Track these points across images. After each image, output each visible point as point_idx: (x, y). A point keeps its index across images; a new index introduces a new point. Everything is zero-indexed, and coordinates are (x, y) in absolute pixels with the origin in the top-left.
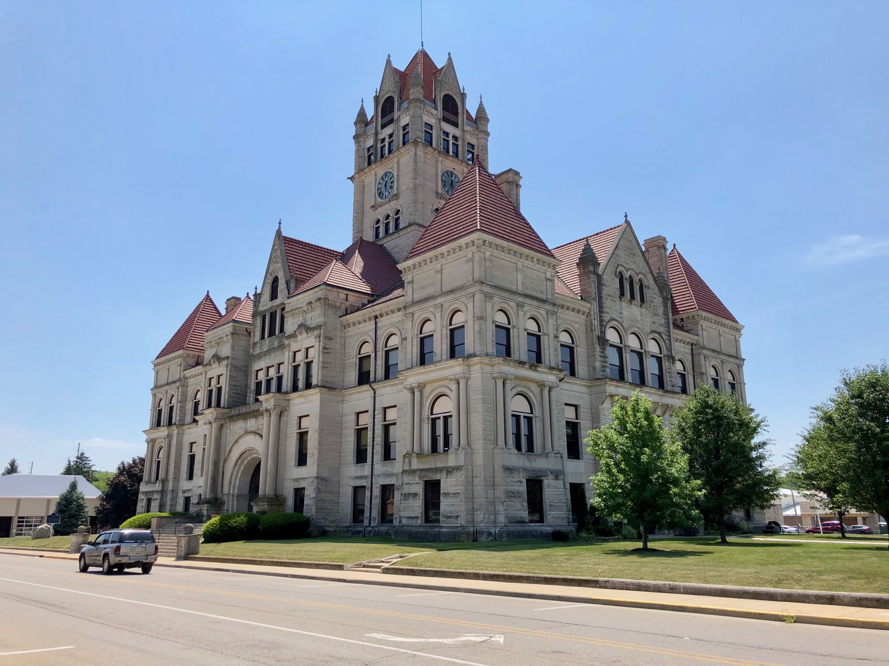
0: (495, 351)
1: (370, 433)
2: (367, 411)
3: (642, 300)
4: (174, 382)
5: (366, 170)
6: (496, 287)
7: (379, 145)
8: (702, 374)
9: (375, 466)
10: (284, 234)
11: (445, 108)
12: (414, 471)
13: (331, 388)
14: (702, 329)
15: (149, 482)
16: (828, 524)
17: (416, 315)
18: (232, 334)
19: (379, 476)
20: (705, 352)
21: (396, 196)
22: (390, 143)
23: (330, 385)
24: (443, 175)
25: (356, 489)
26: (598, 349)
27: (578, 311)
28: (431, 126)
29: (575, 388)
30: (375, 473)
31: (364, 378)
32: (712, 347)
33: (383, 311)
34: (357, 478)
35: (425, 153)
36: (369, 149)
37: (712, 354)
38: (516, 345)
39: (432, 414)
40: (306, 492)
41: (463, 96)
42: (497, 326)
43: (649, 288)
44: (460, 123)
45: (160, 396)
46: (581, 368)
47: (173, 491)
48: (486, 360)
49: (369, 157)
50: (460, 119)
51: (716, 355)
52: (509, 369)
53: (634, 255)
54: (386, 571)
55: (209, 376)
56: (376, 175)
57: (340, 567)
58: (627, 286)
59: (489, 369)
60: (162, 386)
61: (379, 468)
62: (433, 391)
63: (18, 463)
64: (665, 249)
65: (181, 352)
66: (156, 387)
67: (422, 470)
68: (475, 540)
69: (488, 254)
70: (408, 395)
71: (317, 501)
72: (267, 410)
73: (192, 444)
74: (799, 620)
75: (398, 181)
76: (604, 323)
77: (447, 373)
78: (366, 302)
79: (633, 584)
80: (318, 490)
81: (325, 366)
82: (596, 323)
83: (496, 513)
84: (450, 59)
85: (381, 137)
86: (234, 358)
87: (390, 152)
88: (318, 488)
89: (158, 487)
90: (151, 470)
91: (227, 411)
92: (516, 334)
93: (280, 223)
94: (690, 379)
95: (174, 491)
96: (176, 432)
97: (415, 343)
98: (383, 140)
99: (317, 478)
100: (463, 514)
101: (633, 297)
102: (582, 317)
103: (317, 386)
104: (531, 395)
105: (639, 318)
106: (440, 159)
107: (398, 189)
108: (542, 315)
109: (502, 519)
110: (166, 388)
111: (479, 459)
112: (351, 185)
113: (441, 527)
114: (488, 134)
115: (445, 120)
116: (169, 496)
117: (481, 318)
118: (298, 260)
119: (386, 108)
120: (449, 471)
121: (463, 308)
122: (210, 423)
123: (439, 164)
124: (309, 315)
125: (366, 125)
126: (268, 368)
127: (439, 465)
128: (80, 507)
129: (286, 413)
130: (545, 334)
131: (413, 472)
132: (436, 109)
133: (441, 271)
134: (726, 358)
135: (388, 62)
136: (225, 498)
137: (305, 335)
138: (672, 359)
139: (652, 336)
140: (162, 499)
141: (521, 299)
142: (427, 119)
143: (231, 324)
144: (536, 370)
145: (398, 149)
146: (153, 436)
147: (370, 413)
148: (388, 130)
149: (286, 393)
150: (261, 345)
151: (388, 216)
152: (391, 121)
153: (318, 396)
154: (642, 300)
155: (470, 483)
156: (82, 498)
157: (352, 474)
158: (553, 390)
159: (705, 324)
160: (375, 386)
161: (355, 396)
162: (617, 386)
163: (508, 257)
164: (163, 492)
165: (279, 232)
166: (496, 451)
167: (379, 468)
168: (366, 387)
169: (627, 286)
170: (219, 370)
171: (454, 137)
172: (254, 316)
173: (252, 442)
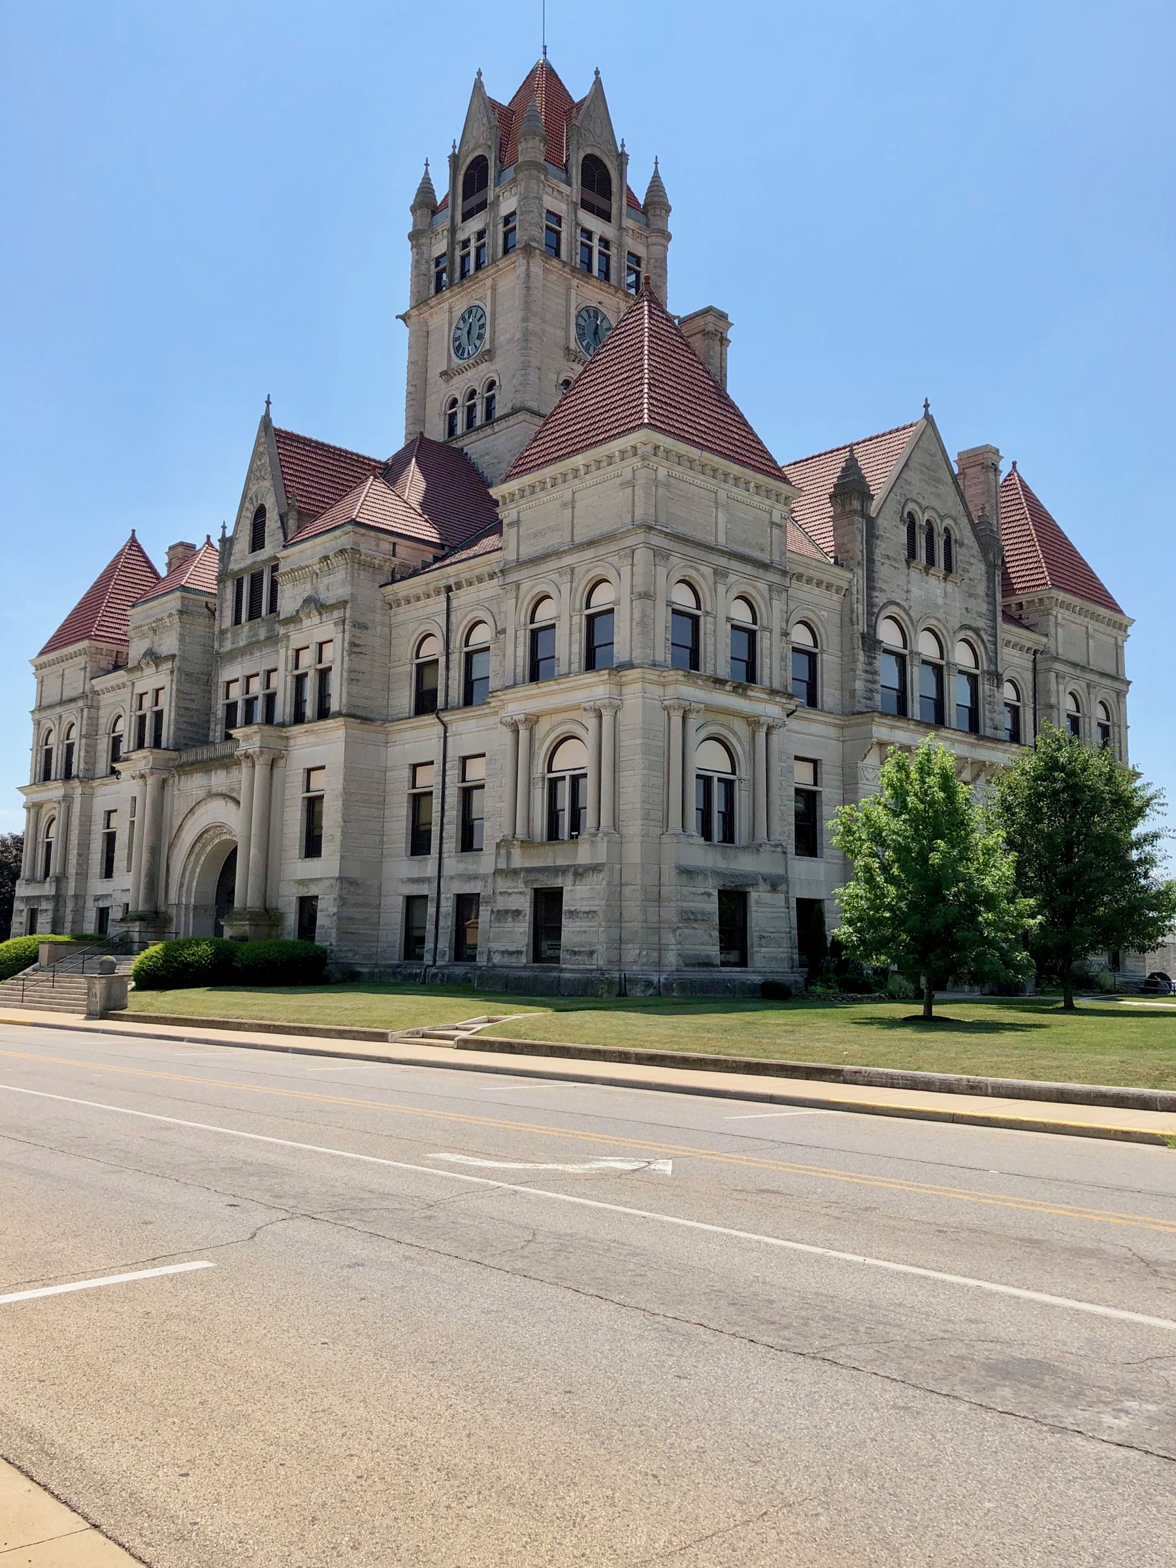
4: (73, 700)
5: (433, 302)
7: (458, 253)
8: (1051, 707)
9: (446, 861)
10: (276, 424)
11: (586, 182)
12: (516, 872)
13: (365, 720)
14: (1057, 624)
15: (31, 880)
19: (452, 878)
20: (1058, 666)
22: (479, 250)
23: (363, 714)
24: (579, 315)
26: (861, 657)
30: (446, 872)
31: (425, 703)
32: (1072, 658)
33: (463, 577)
36: (438, 261)
40: (321, 905)
41: (622, 159)
43: (962, 545)
44: (614, 211)
46: (828, 693)
47: (76, 896)
48: (652, 675)
49: (440, 276)
53: (939, 480)
54: (464, 1045)
55: (139, 690)
57: (382, 1037)
59: (657, 691)
60: (51, 707)
64: (996, 470)
65: (85, 644)
66: (40, 708)
67: (529, 870)
68: (622, 994)
70: (508, 735)
71: (340, 919)
76: (876, 610)
78: (430, 559)
79: (903, 1077)
80: (342, 901)
81: (353, 677)
82: (860, 608)
83: (661, 949)
84: (598, 83)
85: (461, 236)
86: (184, 659)
87: (479, 266)
89: (48, 889)
91: (174, 754)
93: (268, 403)
94: (1027, 716)
96: (79, 791)
98: (466, 244)
99: (340, 879)
100: (601, 949)
101: (931, 561)
102: (836, 597)
103: (339, 714)
104: (733, 740)
105: (940, 601)
106: (575, 282)
107: (492, 340)
108: (762, 596)
110: (58, 710)
111: (634, 853)
112: (403, 333)
113: (561, 970)
114: (668, 237)
115: (587, 205)
118: (303, 475)
119: (473, 178)
120: (579, 872)
122: (143, 776)
123: (573, 292)
126: (248, 678)
127: (561, 862)
129: (281, 763)
130: (764, 629)
133: (573, 504)
135: (478, 86)
136: (173, 911)
137: (316, 619)
138: (996, 678)
140: (56, 911)
141: (723, 561)
143: (178, 594)
147: (438, 766)
149: (283, 725)
151: (473, 394)
152: (482, 206)
153: (341, 733)
154: (949, 568)
157: (403, 874)
158: (775, 732)
159: (1061, 614)
160: (446, 717)
161: (408, 735)
162: (892, 727)
163: (699, 480)
164: (58, 898)
165: (266, 421)
166: (666, 839)
168: (429, 719)
170: (153, 679)
171: (601, 239)
172: (221, 579)
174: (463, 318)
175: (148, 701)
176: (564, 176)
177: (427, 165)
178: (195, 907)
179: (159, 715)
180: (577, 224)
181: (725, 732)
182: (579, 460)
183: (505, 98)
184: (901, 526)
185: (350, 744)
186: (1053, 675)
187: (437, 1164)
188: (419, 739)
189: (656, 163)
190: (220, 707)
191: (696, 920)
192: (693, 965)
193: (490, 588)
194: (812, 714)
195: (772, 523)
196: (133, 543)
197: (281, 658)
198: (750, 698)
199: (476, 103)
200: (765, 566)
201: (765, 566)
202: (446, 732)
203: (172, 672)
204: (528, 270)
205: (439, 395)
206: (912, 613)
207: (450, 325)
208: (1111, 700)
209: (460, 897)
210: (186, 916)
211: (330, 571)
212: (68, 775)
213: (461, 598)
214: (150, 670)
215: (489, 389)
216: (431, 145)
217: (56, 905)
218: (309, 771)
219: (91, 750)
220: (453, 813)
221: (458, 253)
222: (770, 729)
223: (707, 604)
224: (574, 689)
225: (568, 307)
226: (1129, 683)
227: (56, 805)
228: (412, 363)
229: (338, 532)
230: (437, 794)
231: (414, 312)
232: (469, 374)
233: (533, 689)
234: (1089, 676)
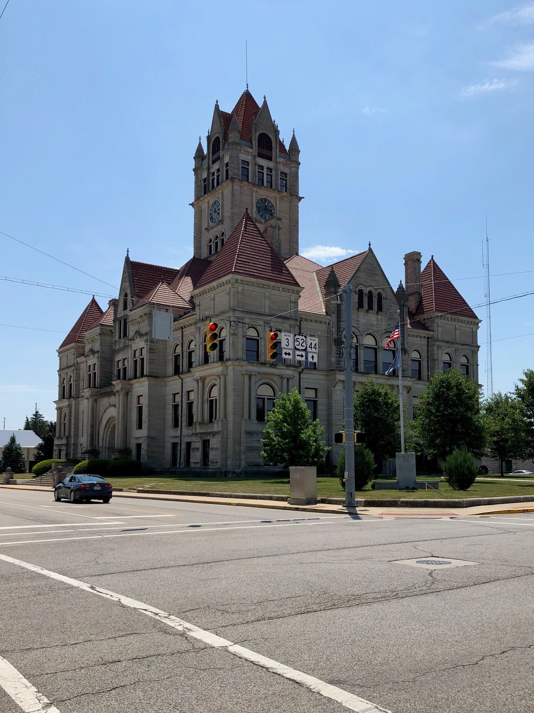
0: (245, 356)
1: (180, 407)
2: (178, 393)
3: (380, 309)
4: (70, 367)
5: (202, 199)
7: (211, 178)
8: (434, 360)
9: (183, 430)
10: (131, 259)
11: (260, 145)
12: (197, 434)
13: (156, 377)
15: (58, 438)
17: (202, 329)
18: (100, 334)
19: (185, 436)
21: (221, 222)
22: (218, 177)
23: (155, 375)
26: (334, 348)
27: (321, 322)
28: (248, 163)
29: (315, 377)
30: (183, 434)
31: (177, 371)
33: (186, 323)
34: (174, 437)
35: (240, 186)
36: (205, 180)
37: (445, 344)
38: (263, 351)
39: (210, 397)
40: (142, 447)
41: (276, 132)
42: (247, 338)
43: (386, 299)
44: (274, 156)
47: (74, 444)
48: (236, 363)
49: (205, 187)
50: (274, 153)
51: (450, 345)
52: (254, 368)
53: (375, 274)
54: (139, 491)
56: (208, 203)
57: (121, 490)
59: (240, 368)
60: (64, 369)
62: (209, 382)
64: (419, 262)
67: (201, 433)
68: (226, 476)
69: (240, 288)
70: (195, 383)
71: (148, 452)
72: (118, 392)
73: (139, 397)
74: (238, 505)
75: (222, 207)
78: (183, 314)
79: (219, 494)
80: (149, 445)
81: (151, 362)
82: (334, 330)
83: (240, 460)
85: (212, 171)
87: (218, 184)
88: (148, 444)
89: (64, 442)
90: (60, 430)
91: (99, 390)
92: (263, 343)
93: (128, 251)
94: (424, 364)
96: (74, 403)
97: (201, 348)
98: (213, 174)
99: (148, 437)
100: (219, 461)
101: (370, 307)
103: (147, 376)
105: (375, 323)
106: (255, 189)
107: (222, 215)
110: (66, 370)
111: (231, 427)
112: (192, 210)
113: (209, 469)
114: (299, 164)
115: (260, 155)
116: (72, 448)
117: (234, 334)
119: (216, 143)
120: (214, 434)
121: (193, 339)
122: (88, 398)
123: (254, 193)
124: (142, 325)
125: (203, 160)
126: (124, 359)
128: (19, 455)
129: (130, 393)
132: (252, 148)
133: (214, 299)
134: (460, 347)
135: (217, 107)
136: (100, 450)
137: (139, 339)
140: (67, 450)
142: (243, 157)
143: (99, 327)
144: (275, 368)
145: (222, 182)
146: (61, 405)
148: (216, 166)
149: (130, 379)
150: (120, 342)
151: (217, 237)
152: (218, 159)
153: (147, 383)
154: (380, 309)
156: (20, 449)
157: (171, 434)
158: (290, 380)
159: (440, 322)
161: (172, 382)
163: (257, 289)
164: (67, 445)
165: (127, 259)
166: (243, 422)
168: (176, 377)
170: (93, 360)
171: (267, 168)
173: (112, 412)
174: (213, 206)
175: (138, 353)
176: (249, 144)
177: (200, 139)
178: (108, 448)
179: (142, 360)
180: (256, 164)
181: (269, 381)
182: (214, 284)
184: (355, 295)
185: (151, 388)
186: (436, 347)
187: (42, 507)
188: (174, 385)
189: (294, 131)
190: (115, 371)
191: (253, 450)
192: (252, 466)
193: (192, 329)
195: (291, 302)
196: (94, 301)
197: (129, 354)
198: (277, 368)
199: (216, 115)
202: (182, 382)
203: (98, 358)
204: (233, 187)
205: (206, 237)
206: (359, 329)
207: (208, 208)
208: (469, 355)
210: (105, 451)
211: (143, 321)
212: (70, 396)
213: (186, 331)
215: (222, 236)
217: (67, 447)
219: (78, 386)
220: (185, 412)
221: (211, 178)
222: (288, 380)
223: (261, 335)
224: (213, 368)
225: (252, 200)
226: (479, 347)
228: (195, 224)
229: (144, 307)
230: (180, 405)
231: (196, 203)
232: (215, 229)
234: (455, 346)
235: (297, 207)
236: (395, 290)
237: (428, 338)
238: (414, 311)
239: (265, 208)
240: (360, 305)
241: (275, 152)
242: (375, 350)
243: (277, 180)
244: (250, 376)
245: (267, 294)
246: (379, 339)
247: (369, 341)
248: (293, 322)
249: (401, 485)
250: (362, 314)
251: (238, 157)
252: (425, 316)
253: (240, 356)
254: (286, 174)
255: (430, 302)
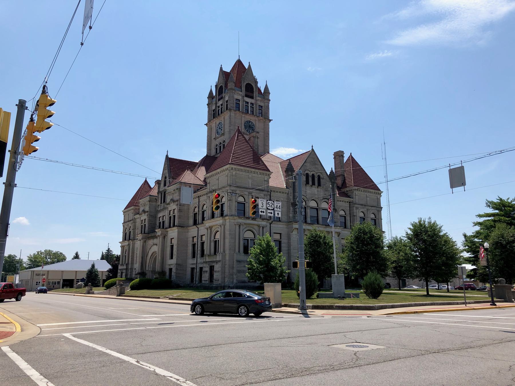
0: (236, 213)
3: (319, 185)
5: (212, 121)
6: (238, 187)
7: (217, 109)
10: (169, 157)
16: (466, 285)
18: (149, 201)
20: (356, 206)
22: (221, 108)
24: (245, 123)
25: (193, 269)
26: (291, 208)
27: (283, 193)
30: (198, 262)
31: (195, 223)
32: (361, 203)
36: (214, 111)
37: (361, 206)
41: (256, 82)
43: (323, 179)
44: (254, 96)
45: (126, 226)
48: (231, 218)
49: (214, 114)
50: (254, 95)
53: (316, 164)
54: (170, 299)
55: (169, 210)
57: (159, 298)
58: (310, 179)
59: (233, 221)
61: (199, 260)
63: (79, 253)
64: (343, 157)
65: (133, 207)
66: (124, 223)
67: (209, 262)
69: (234, 173)
77: (218, 223)
80: (177, 269)
81: (179, 217)
82: (291, 197)
84: (250, 65)
85: (218, 105)
87: (222, 112)
89: (125, 267)
94: (348, 218)
95: (132, 269)
98: (219, 107)
100: (220, 279)
101: (313, 184)
102: (285, 195)
103: (176, 226)
104: (254, 230)
105: (316, 193)
106: (243, 115)
109: (235, 281)
112: (206, 128)
115: (247, 96)
116: (129, 271)
117: (230, 200)
118: (175, 167)
119: (220, 89)
120: (217, 262)
124: (175, 195)
127: (214, 260)
128: (97, 275)
131: (206, 262)
132: (242, 91)
134: (370, 208)
136: (147, 272)
139: (324, 200)
140: (126, 272)
142: (236, 97)
145: (224, 111)
146: (123, 245)
147: (197, 237)
148: (220, 102)
152: (222, 98)
153: (177, 230)
154: (319, 185)
155: (223, 267)
156: (97, 271)
157: (191, 262)
159: (357, 193)
160: (198, 226)
161: (192, 230)
163: (244, 173)
165: (167, 156)
167: (199, 260)
168: (195, 227)
169: (310, 179)
170: (144, 217)
172: (158, 193)
173: (155, 249)
181: (251, 229)
182: (219, 170)
183: (228, 70)
186: (355, 208)
188: (193, 231)
194: (279, 223)
196: (146, 181)
197: (166, 213)
200: (263, 191)
201: (263, 191)
205: (214, 143)
208: (376, 213)
209: (293, 262)
211: (176, 193)
213: (202, 199)
214: (143, 215)
216: (212, 80)
218: (172, 239)
219: (134, 233)
220: (199, 248)
221: (217, 109)
227: (219, 227)
233: (213, 220)
235: (268, 125)
236: (328, 173)
237: (350, 202)
238: (340, 186)
239: (249, 126)
240: (307, 182)
241: (256, 94)
242: (317, 209)
243: (256, 110)
244: (240, 226)
245: (250, 176)
246: (319, 203)
247: (313, 204)
248: (266, 193)
249: (335, 295)
250: (308, 187)
251: (233, 97)
252: (347, 189)
253: (233, 213)
254: (262, 107)
255: (350, 180)
